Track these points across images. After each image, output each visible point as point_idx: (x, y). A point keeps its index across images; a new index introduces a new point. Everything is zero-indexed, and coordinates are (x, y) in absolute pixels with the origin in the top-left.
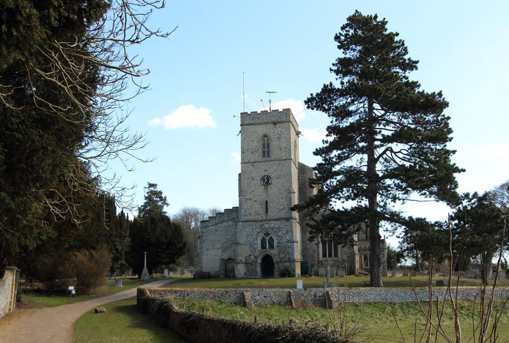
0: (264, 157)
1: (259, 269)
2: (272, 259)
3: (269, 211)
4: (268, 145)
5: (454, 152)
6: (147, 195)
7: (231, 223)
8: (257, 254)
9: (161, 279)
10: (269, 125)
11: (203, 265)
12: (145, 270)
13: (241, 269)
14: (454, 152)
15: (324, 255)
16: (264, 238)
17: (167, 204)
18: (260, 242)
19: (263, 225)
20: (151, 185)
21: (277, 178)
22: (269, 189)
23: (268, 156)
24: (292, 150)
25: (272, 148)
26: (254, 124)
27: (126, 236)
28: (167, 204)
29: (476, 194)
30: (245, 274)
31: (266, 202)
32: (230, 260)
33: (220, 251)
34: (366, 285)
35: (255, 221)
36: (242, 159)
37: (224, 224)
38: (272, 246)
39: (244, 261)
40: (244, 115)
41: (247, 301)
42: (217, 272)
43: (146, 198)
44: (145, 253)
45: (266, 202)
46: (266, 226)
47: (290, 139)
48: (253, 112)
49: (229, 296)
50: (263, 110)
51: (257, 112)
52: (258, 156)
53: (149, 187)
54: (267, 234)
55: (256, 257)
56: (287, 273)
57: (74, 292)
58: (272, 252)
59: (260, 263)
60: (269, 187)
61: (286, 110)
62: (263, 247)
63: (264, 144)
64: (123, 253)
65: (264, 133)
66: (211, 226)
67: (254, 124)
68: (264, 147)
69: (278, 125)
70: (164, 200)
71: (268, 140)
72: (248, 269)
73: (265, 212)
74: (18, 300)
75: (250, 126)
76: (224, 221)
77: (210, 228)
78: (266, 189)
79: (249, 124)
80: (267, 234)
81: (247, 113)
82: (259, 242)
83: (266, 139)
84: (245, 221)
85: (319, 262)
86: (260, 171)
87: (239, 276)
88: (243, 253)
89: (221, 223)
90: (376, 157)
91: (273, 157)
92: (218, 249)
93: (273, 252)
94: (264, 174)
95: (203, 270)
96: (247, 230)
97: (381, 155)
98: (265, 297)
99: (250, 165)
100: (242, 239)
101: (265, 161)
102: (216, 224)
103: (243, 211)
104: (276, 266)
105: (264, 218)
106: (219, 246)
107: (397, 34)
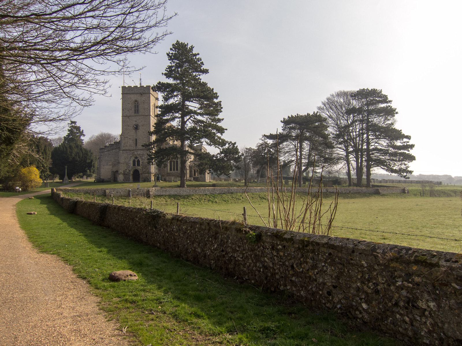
1: (131, 177)
2: (139, 172)
3: (138, 144)
4: (138, 106)
5: (223, 119)
6: (70, 129)
7: (118, 150)
8: (130, 169)
13: (121, 177)
14: (223, 119)
15: (171, 169)
16: (134, 160)
17: (84, 135)
18: (132, 162)
19: (134, 153)
20: (72, 122)
23: (138, 113)
24: (151, 110)
25: (140, 109)
27: (49, 159)
28: (84, 135)
29: (231, 142)
30: (123, 180)
31: (136, 139)
32: (117, 171)
34: (178, 186)
35: (129, 150)
36: (123, 114)
37: (114, 151)
38: (138, 165)
40: (124, 88)
41: (107, 194)
42: (109, 179)
43: (69, 131)
44: (66, 167)
45: (136, 139)
46: (136, 153)
47: (150, 103)
49: (98, 192)
51: (131, 86)
53: (71, 123)
54: (136, 158)
55: (129, 171)
56: (148, 180)
59: (132, 174)
61: (148, 86)
62: (134, 165)
63: (135, 106)
64: (48, 168)
65: (136, 99)
66: (106, 152)
69: (143, 95)
70: (82, 134)
71: (137, 103)
73: (135, 145)
79: (126, 94)
80: (136, 158)
81: (125, 87)
82: (131, 162)
83: (136, 103)
84: (124, 150)
85: (168, 173)
87: (120, 181)
88: (122, 168)
89: (112, 150)
91: (140, 114)
93: (139, 168)
94: (134, 123)
95: (101, 178)
96: (125, 155)
97: (188, 120)
98: (117, 192)
100: (122, 160)
101: (136, 116)
102: (109, 151)
103: (123, 144)
104: (141, 176)
105: (135, 148)
106: (111, 163)
107: (198, 54)
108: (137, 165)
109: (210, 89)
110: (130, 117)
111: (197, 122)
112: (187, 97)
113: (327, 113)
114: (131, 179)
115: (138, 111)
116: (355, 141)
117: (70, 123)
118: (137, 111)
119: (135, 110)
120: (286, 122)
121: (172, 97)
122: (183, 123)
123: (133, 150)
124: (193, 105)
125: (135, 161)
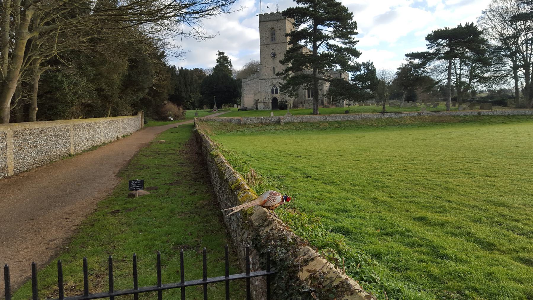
0: (272, 41)
1: (270, 105)
8: (269, 97)
9: (472, 121)
10: (275, 21)
11: (245, 103)
12: (215, 107)
15: (309, 97)
16: (273, 88)
19: (272, 81)
20: (220, 53)
21: (279, 54)
22: (275, 61)
23: (275, 41)
25: (276, 36)
26: (266, 21)
30: (264, 108)
31: (274, 68)
33: (253, 95)
34: (311, 114)
37: (255, 80)
39: (263, 101)
40: (261, 16)
45: (274, 68)
46: (274, 82)
47: (286, 30)
48: (266, 14)
50: (271, 12)
51: (267, 14)
52: (269, 41)
54: (274, 86)
57: (172, 119)
58: (277, 96)
60: (275, 59)
62: (273, 93)
63: (272, 33)
67: (266, 21)
68: (272, 35)
69: (279, 21)
71: (274, 30)
72: (265, 106)
74: (145, 122)
75: (264, 23)
76: (255, 78)
77: (248, 82)
78: (273, 60)
81: (262, 14)
82: (270, 90)
83: (273, 30)
84: (263, 79)
86: (270, 51)
89: (253, 79)
90: (317, 46)
91: (277, 41)
92: (252, 94)
95: (245, 106)
99: (264, 46)
102: (251, 80)
106: (253, 92)
108: (276, 94)
109: (346, 8)
110: (267, 46)
111: (330, 46)
112: (319, 20)
113: (491, 23)
114: (270, 107)
115: (275, 39)
116: (525, 54)
117: (218, 53)
118: (273, 39)
119: (272, 38)
120: (433, 38)
121: (301, 22)
122: (316, 48)
123: (271, 79)
124: (327, 30)
125: (274, 89)
